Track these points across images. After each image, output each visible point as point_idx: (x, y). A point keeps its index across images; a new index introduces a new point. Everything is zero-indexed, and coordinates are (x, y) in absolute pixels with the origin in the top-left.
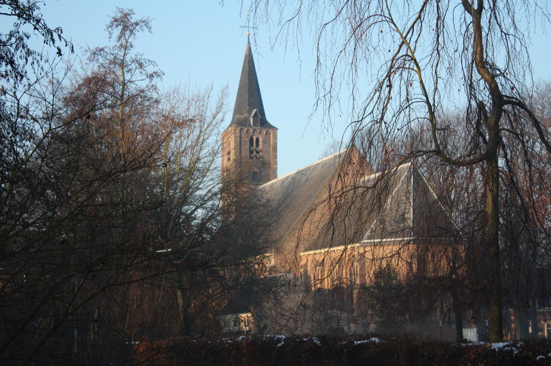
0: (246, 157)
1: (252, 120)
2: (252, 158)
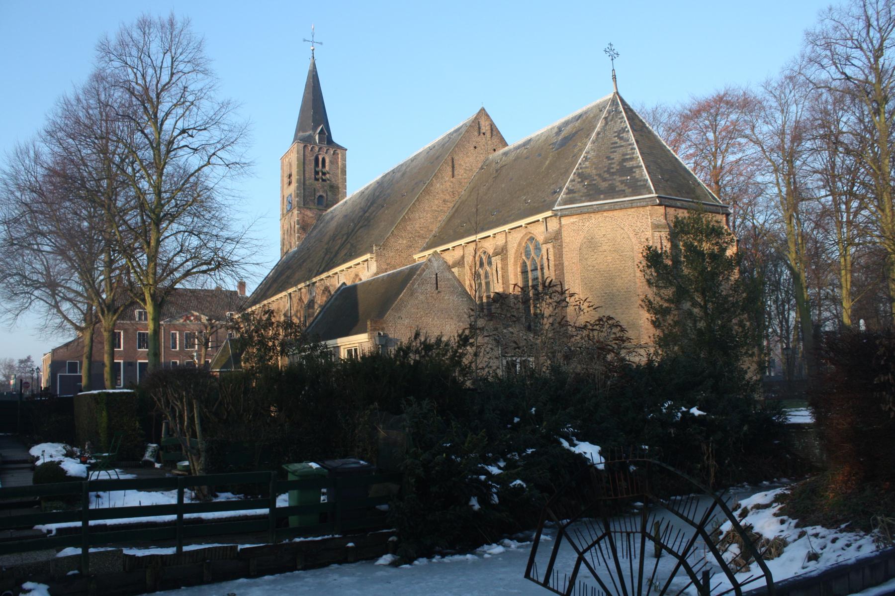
0: (310, 179)
1: (317, 137)
2: (317, 180)
